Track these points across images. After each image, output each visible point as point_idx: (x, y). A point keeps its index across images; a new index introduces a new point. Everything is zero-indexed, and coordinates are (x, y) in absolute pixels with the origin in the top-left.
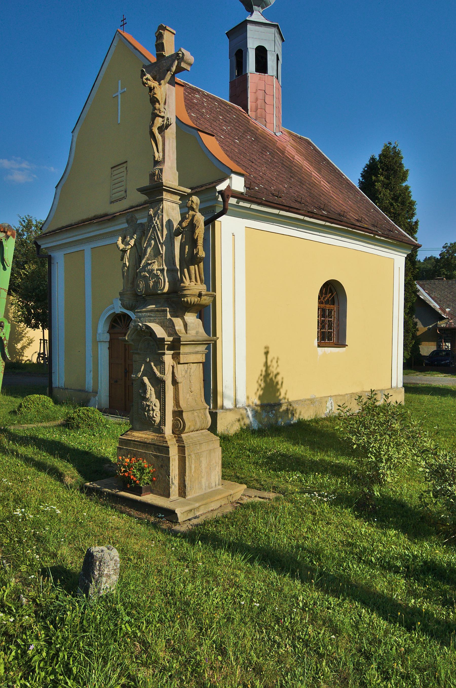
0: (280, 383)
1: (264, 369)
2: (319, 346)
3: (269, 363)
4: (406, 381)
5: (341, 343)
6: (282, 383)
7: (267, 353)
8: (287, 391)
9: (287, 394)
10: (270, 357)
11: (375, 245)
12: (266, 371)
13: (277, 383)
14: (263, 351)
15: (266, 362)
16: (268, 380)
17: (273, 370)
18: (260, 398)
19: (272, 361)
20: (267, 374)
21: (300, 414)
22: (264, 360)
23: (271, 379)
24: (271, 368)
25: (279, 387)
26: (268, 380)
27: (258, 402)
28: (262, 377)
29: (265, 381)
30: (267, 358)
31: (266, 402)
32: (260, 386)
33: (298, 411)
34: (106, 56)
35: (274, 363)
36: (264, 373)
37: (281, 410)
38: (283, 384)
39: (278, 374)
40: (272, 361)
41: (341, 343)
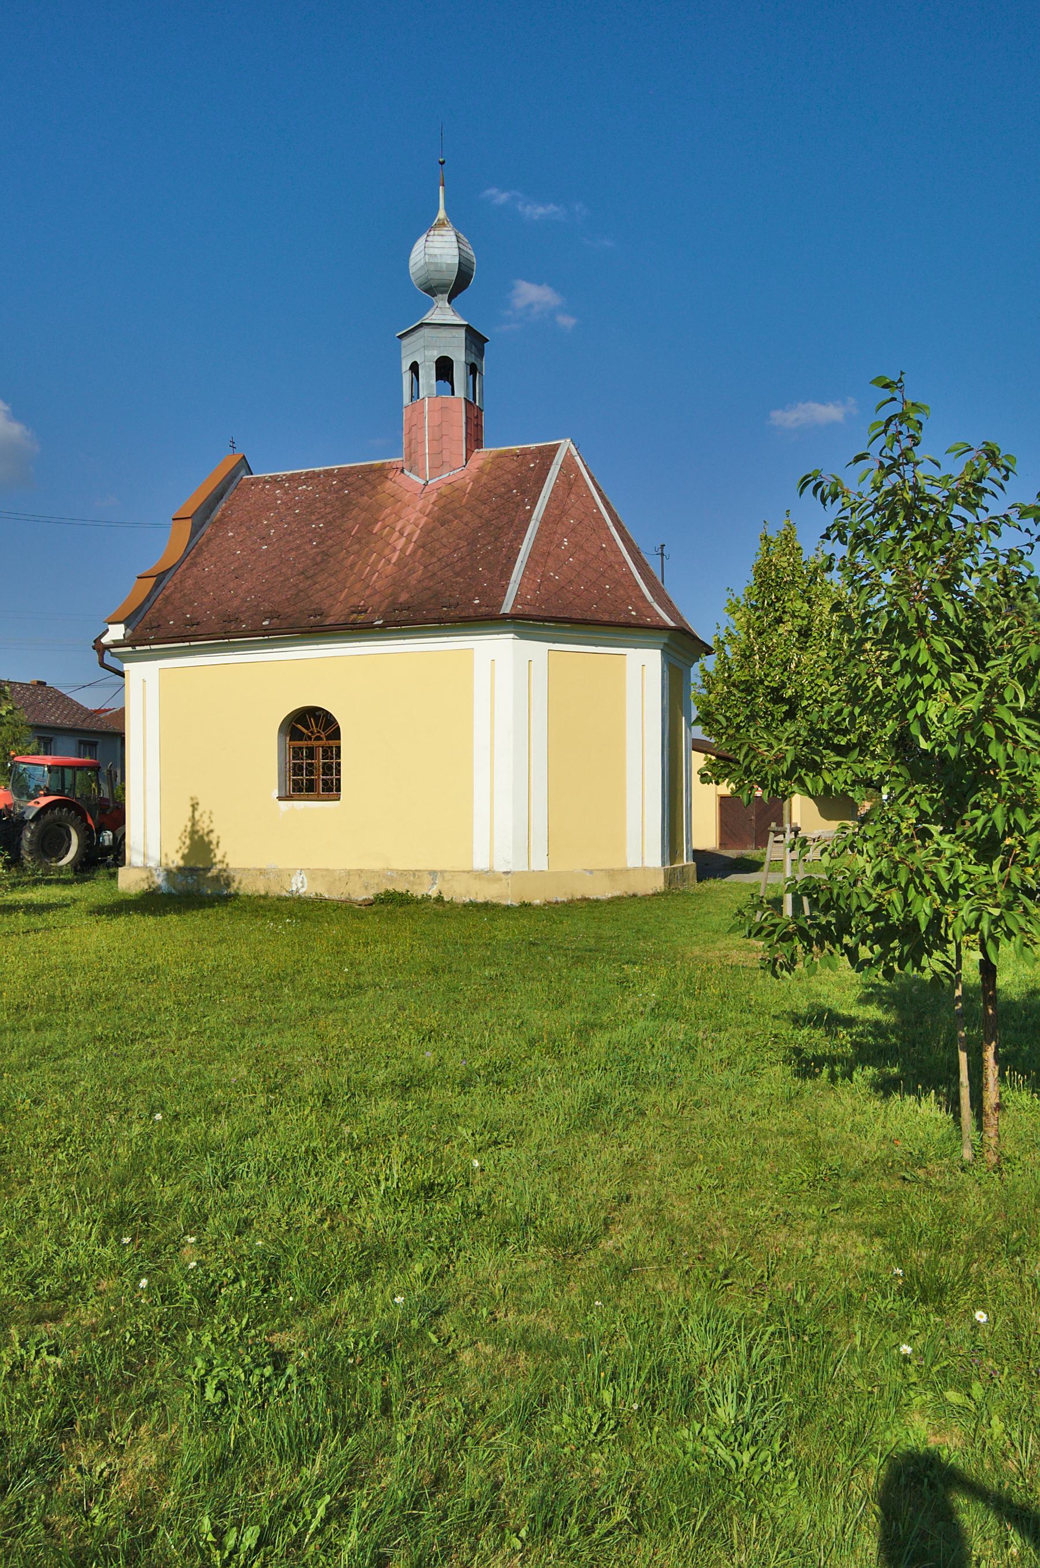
0: (215, 842)
1: (189, 824)
2: (280, 798)
3: (197, 816)
4: (113, 882)
5: (331, 789)
6: (218, 843)
7: (194, 807)
8: (801, 493)
9: (227, 856)
10: (200, 809)
11: (404, 639)
12: (193, 825)
13: (210, 843)
14: (190, 803)
15: (193, 816)
16: (196, 837)
17: (203, 826)
18: (184, 857)
19: (201, 816)
20: (194, 832)
21: (240, 883)
22: (190, 814)
23: (201, 837)
24: (200, 823)
25: (212, 847)
26: (196, 837)
27: (181, 863)
28: (187, 834)
29: (191, 839)
30: (193, 812)
31: (192, 864)
32: (184, 843)
33: (237, 879)
34: (145, 793)
35: (205, 817)
36: (189, 829)
37: (210, 875)
38: (220, 845)
39: (212, 831)
40: (201, 816)
41: (331, 789)
